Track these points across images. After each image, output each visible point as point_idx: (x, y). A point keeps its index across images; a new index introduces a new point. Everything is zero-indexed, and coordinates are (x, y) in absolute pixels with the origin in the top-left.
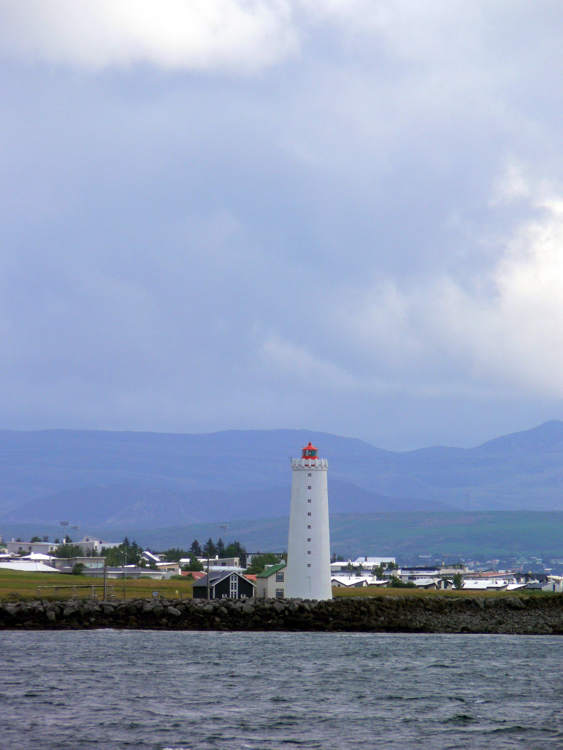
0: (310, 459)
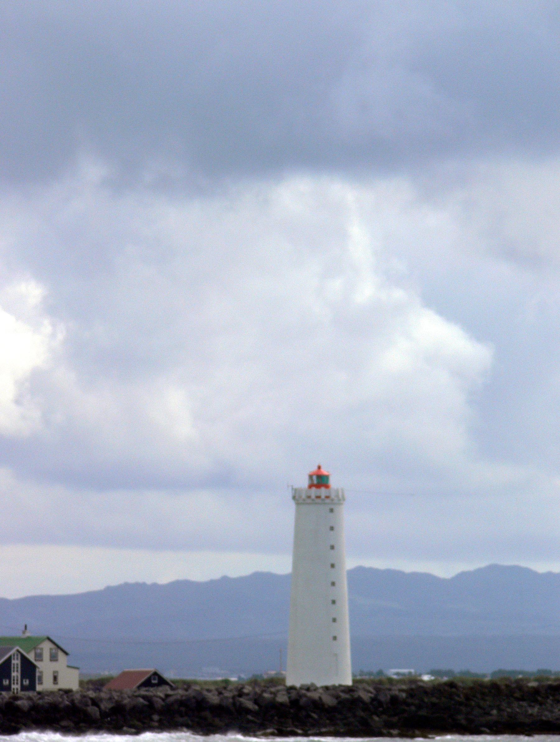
0: (323, 489)
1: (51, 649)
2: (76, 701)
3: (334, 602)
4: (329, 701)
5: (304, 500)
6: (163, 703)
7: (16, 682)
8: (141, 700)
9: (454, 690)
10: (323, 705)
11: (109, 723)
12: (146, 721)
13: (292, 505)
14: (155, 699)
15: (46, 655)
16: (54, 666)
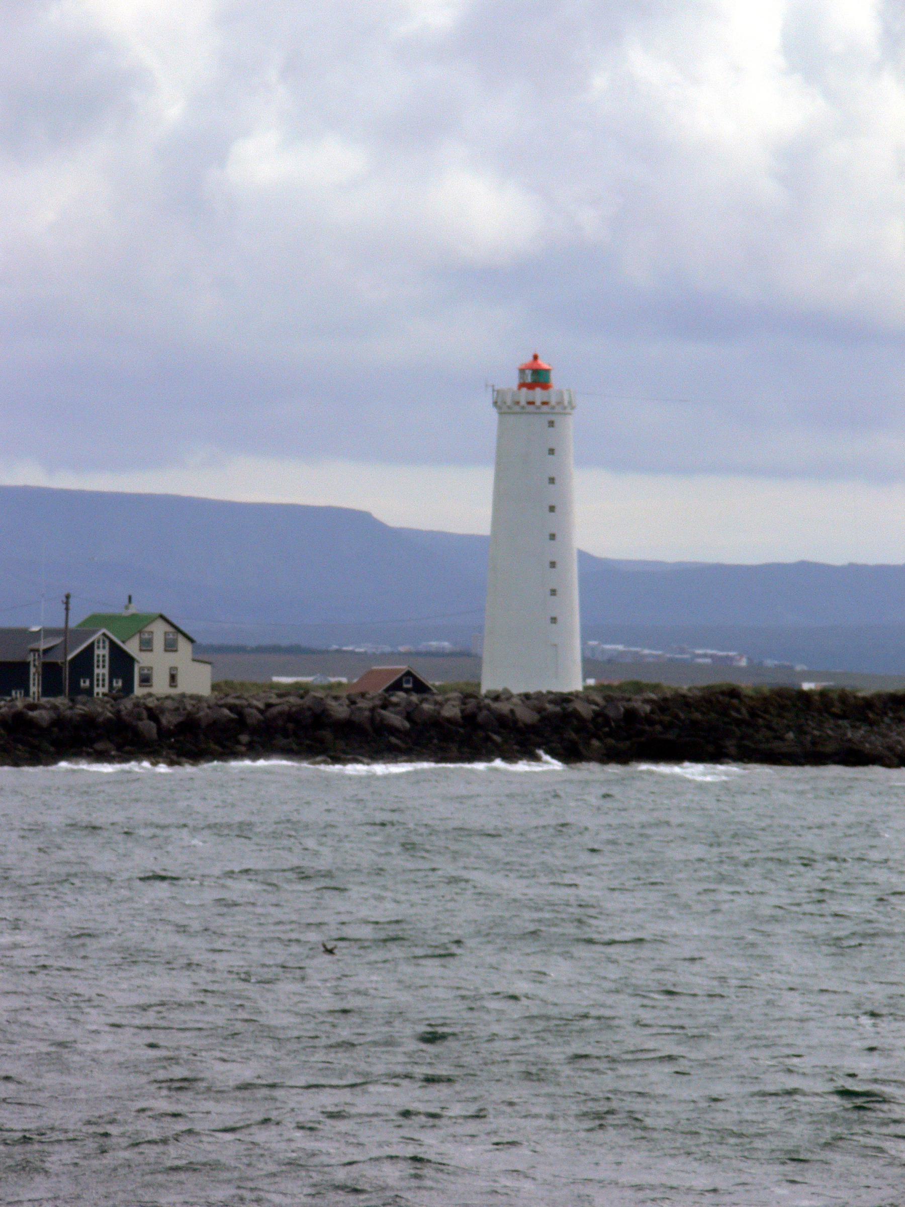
0: (538, 390)
1: (166, 633)
2: (124, 713)
3: (553, 565)
4: (526, 716)
5: (509, 407)
6: (261, 717)
7: (101, 682)
8: (226, 711)
9: (735, 701)
10: (516, 722)
11: (171, 747)
12: (228, 744)
13: (493, 413)
14: (248, 711)
15: (158, 643)
16: (171, 659)
